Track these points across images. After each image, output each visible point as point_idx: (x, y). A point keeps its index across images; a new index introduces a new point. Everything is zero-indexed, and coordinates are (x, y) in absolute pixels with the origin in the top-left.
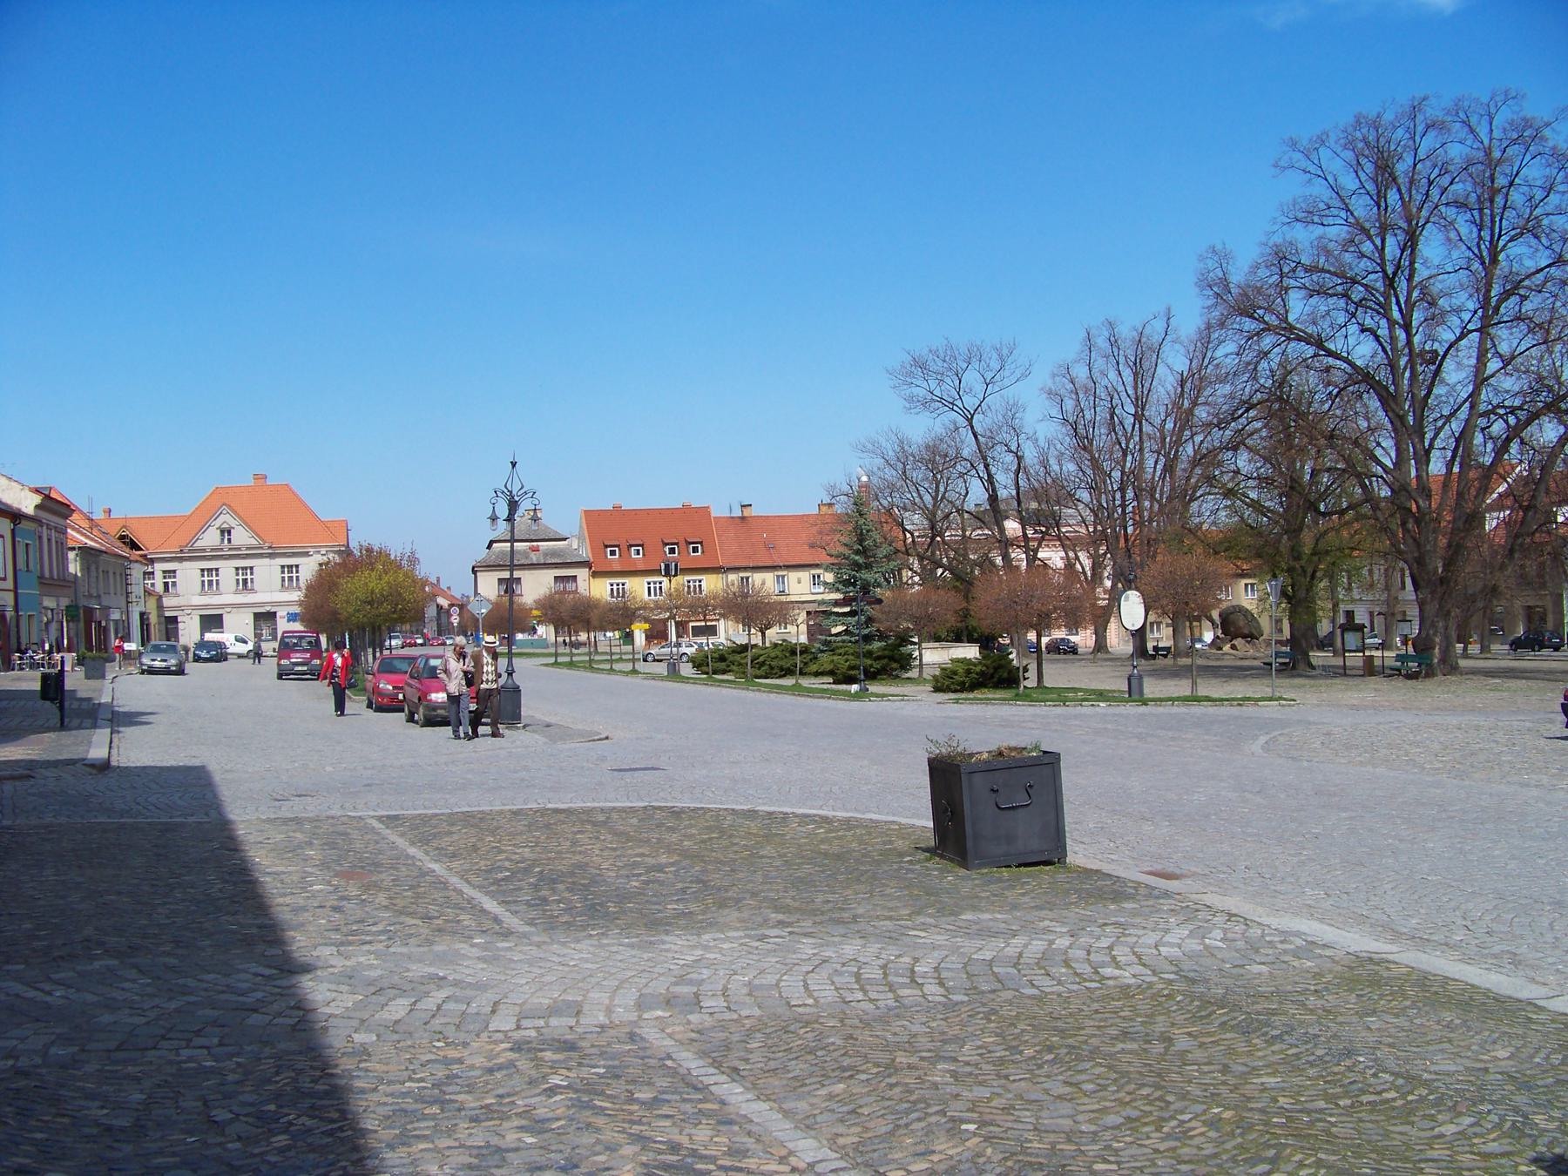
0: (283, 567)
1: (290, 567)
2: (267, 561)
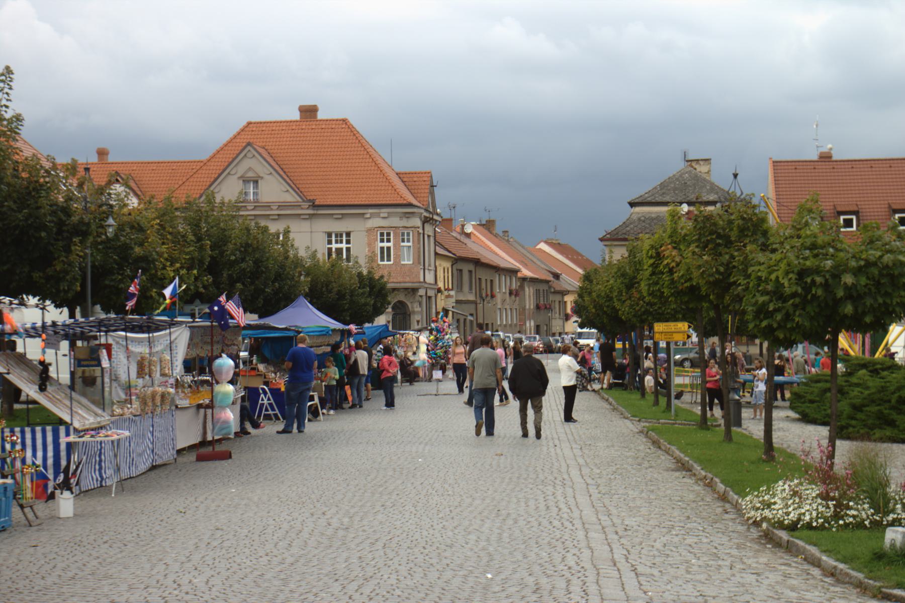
0: (329, 235)
1: (339, 235)
2: (305, 225)
